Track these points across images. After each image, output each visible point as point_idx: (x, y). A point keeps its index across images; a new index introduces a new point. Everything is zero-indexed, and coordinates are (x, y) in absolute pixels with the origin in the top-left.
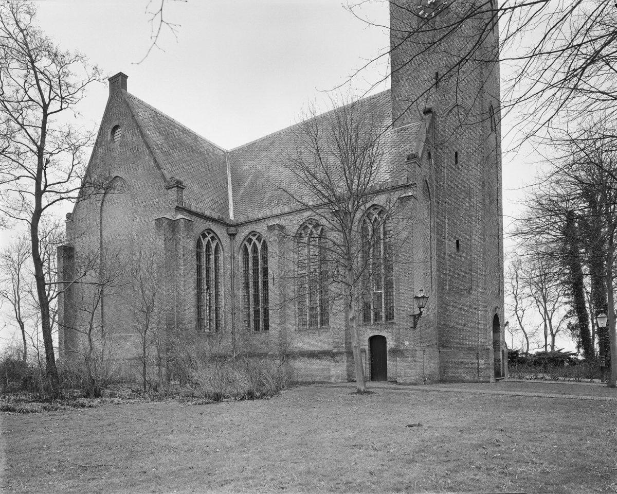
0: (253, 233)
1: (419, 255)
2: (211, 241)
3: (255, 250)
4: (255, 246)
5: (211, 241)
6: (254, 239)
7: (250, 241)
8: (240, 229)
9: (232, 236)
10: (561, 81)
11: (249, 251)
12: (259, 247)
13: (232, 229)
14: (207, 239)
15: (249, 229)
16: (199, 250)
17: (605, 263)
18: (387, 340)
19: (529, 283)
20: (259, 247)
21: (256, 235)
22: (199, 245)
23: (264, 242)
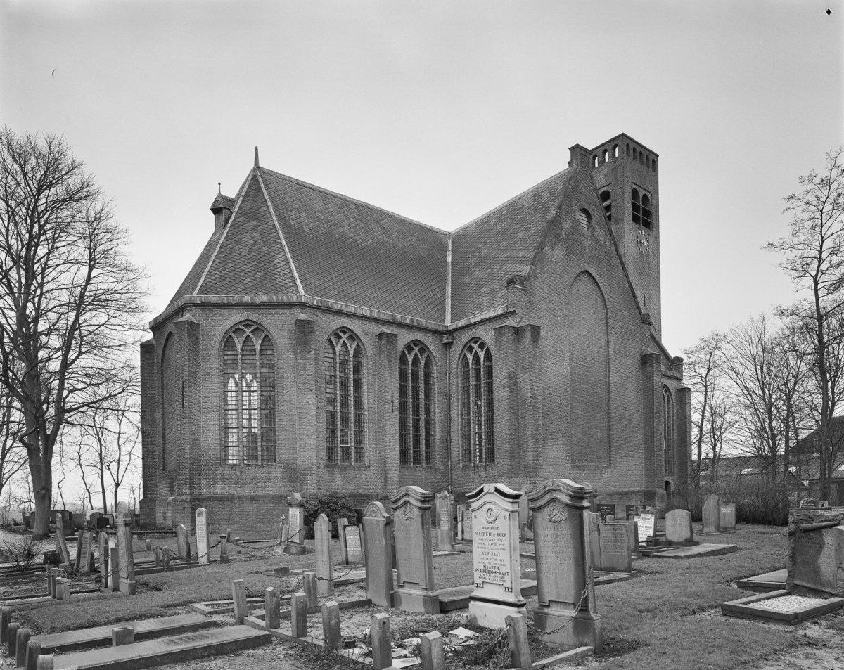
0: (475, 340)
1: (177, 647)
2: (419, 354)
3: (476, 357)
4: (476, 354)
5: (419, 354)
6: (475, 346)
7: (471, 349)
8: (455, 335)
9: (448, 345)
10: (663, 557)
11: (482, 358)
12: (482, 355)
13: (446, 337)
14: (413, 353)
15: (466, 337)
16: (489, 363)
17: (41, 456)
18: (542, 333)
19: (190, 299)
20: (482, 355)
21: (477, 342)
22: (403, 360)
23: (488, 349)
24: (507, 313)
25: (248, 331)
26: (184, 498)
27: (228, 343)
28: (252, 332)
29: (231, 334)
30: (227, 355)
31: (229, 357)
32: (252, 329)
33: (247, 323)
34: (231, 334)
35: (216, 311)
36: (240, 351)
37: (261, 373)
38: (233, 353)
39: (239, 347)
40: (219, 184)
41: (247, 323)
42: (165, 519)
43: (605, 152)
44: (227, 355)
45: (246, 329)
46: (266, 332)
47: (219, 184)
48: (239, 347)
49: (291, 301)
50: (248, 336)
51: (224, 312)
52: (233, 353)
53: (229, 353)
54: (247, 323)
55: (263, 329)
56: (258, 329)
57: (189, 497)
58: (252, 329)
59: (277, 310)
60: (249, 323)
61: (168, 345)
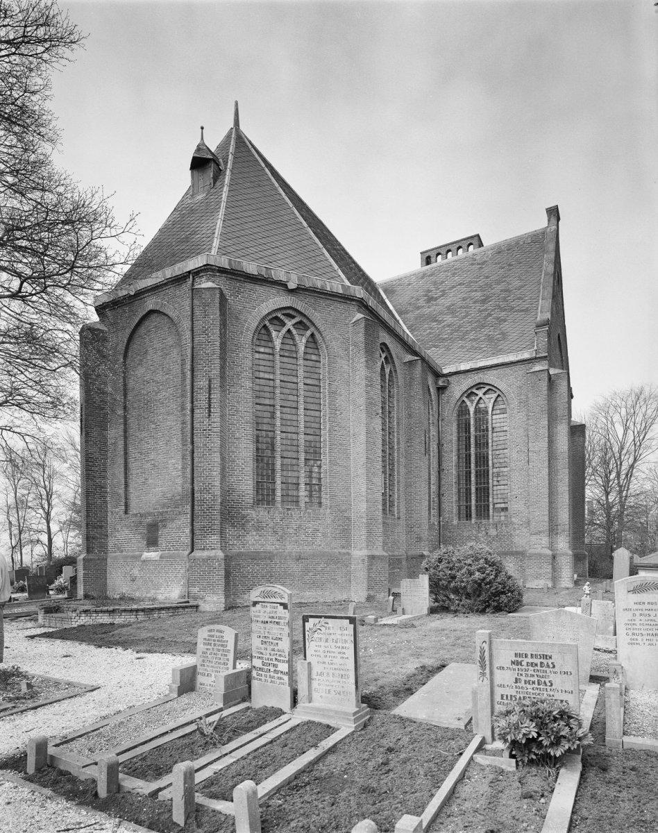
24: (536, 358)
25: (289, 324)
26: (212, 553)
27: (263, 332)
28: (484, 394)
29: (267, 323)
30: (259, 352)
31: (262, 356)
32: (294, 321)
33: (290, 312)
34: (267, 323)
35: (249, 286)
36: (278, 347)
37: (273, 355)
38: (267, 350)
39: (277, 343)
40: (202, 128)
41: (288, 311)
42: (179, 476)
43: (449, 251)
44: (259, 352)
45: (286, 321)
46: (312, 329)
47: (202, 128)
48: (277, 343)
49: (348, 293)
50: (289, 331)
51: (260, 289)
52: (267, 350)
53: (262, 350)
54: (288, 311)
55: (308, 324)
56: (491, 388)
57: (220, 554)
58: (294, 321)
59: (328, 302)
60: (291, 312)
61: (135, 346)
